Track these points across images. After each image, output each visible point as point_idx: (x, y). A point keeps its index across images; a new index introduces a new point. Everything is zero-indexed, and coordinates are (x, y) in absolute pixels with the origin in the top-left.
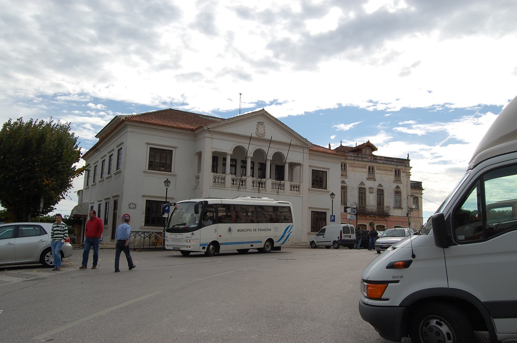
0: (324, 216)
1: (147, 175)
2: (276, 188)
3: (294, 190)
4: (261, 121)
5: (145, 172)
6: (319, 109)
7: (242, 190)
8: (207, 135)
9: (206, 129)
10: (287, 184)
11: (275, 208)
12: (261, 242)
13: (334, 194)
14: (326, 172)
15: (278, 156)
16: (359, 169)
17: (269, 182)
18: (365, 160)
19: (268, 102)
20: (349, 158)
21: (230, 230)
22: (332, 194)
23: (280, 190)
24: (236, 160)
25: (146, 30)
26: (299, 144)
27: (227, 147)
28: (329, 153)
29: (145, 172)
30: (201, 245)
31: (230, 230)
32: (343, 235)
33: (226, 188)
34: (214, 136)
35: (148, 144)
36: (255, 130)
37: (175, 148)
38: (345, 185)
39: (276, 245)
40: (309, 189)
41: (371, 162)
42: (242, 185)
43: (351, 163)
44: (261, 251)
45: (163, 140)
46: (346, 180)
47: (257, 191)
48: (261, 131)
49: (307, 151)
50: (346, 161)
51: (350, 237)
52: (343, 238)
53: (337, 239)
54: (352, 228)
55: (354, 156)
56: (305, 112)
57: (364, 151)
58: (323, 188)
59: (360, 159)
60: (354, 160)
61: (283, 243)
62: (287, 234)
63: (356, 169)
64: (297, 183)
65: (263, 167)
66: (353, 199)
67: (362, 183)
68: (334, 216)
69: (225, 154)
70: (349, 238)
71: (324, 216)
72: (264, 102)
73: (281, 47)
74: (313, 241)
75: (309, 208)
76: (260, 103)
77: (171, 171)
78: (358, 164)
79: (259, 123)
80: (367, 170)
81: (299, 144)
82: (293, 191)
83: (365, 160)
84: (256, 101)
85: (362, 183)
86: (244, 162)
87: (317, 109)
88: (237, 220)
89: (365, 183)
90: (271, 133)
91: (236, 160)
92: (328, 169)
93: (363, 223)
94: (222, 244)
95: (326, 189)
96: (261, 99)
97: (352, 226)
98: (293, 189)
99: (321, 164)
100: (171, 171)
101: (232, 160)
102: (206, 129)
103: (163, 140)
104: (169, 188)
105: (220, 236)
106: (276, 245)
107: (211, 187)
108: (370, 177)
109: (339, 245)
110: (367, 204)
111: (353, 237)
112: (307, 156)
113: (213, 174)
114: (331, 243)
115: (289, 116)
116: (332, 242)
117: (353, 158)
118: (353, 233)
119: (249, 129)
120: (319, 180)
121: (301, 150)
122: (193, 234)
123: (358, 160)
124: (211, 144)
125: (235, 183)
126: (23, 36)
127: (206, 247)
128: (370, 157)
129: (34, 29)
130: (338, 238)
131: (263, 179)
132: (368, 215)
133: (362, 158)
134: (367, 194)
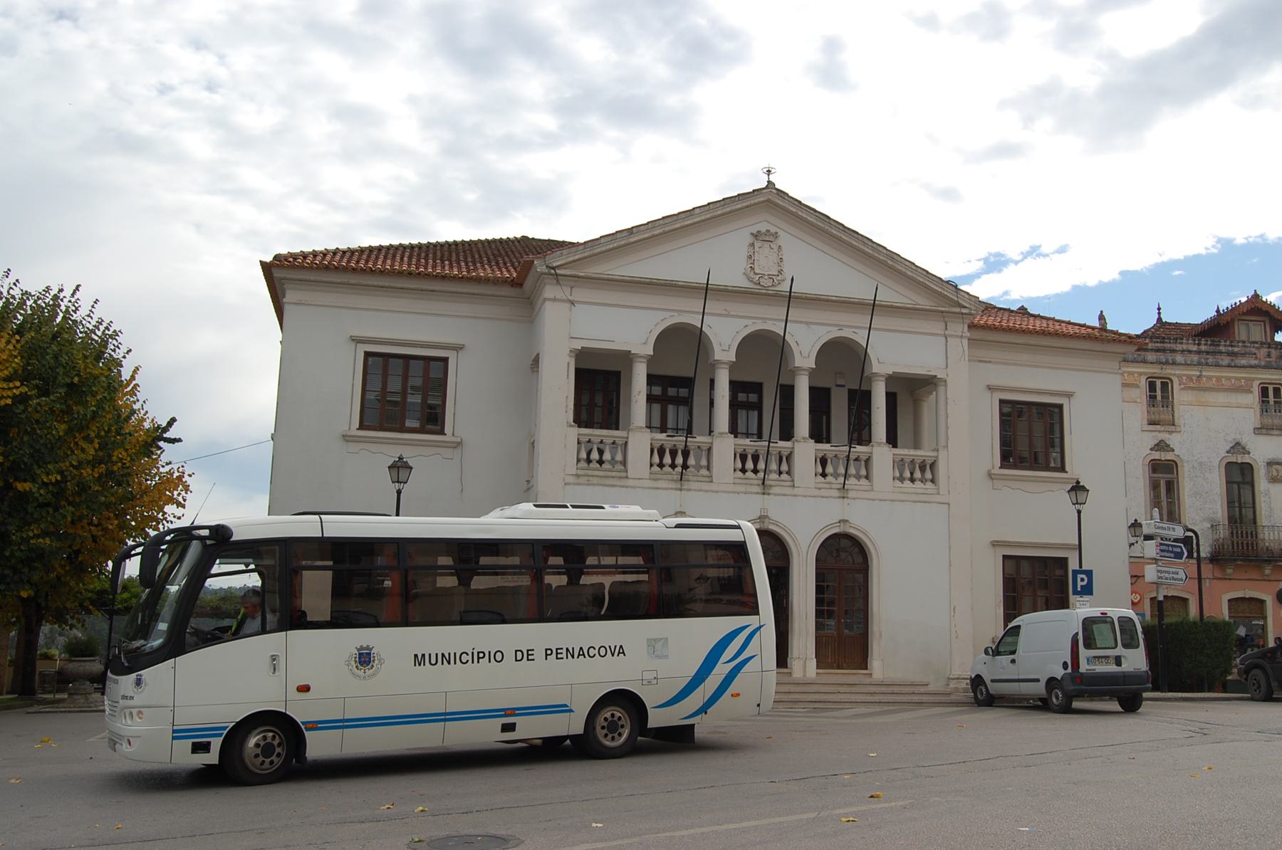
0: (1059, 572)
1: (353, 447)
2: (836, 475)
3: (923, 480)
4: (763, 227)
5: (347, 438)
6: (1165, 259)
7: (693, 485)
8: (550, 291)
9: (544, 269)
10: (882, 455)
11: (645, 551)
12: (563, 709)
13: (1084, 489)
14: (1060, 407)
15: (843, 355)
16: (1221, 398)
17: (639, 439)
18: (1244, 362)
19: (1013, 254)
20: (1179, 358)
21: (365, 658)
22: (1077, 488)
23: (852, 481)
24: (757, 388)
25: (672, 101)
26: (924, 302)
27: (631, 330)
28: (1065, 336)
29: (347, 438)
30: (178, 734)
31: (365, 658)
32: (1084, 653)
33: (630, 482)
34: (579, 294)
35: (357, 341)
36: (743, 264)
37: (458, 348)
38: (1169, 456)
39: (656, 719)
40: (990, 476)
41: (1268, 367)
42: (698, 467)
43: (1190, 378)
44: (576, 749)
45: (410, 325)
46: (1173, 440)
47: (758, 489)
48: (766, 261)
49: (959, 328)
50: (1169, 371)
51: (1118, 661)
52: (1084, 667)
53: (1059, 673)
54: (1126, 623)
55: (1199, 352)
56: (1122, 273)
57: (1241, 331)
58: (1048, 469)
59: (1226, 360)
60: (1199, 364)
61: (704, 709)
62: (721, 670)
63: (1211, 397)
64: (924, 453)
65: (746, 395)
66: (1204, 505)
67: (1238, 447)
68: (1089, 573)
69: (627, 358)
70: (1112, 668)
71: (1059, 572)
72: (1002, 255)
73: (1043, 99)
74: (978, 676)
75: (995, 544)
76: (992, 259)
77: (442, 432)
78: (1219, 379)
79: (756, 236)
80: (1253, 398)
81: (924, 302)
82: (918, 484)
83: (1244, 362)
84: (983, 255)
85: (1238, 447)
86: (787, 394)
87: (1159, 260)
88: (413, 608)
89: (1249, 447)
90: (811, 271)
91: (757, 388)
92: (1069, 395)
93: (1249, 594)
94: (314, 726)
95: (1062, 469)
96: (993, 250)
97: (1130, 613)
98: (918, 474)
99: (1034, 378)
100: (442, 432)
101: (735, 386)
102: (544, 269)
103: (410, 325)
104: (406, 489)
105: (305, 689)
106: (656, 719)
107: (571, 479)
108: (1268, 421)
109: (1069, 698)
110: (1263, 520)
111: (1136, 660)
112: (959, 347)
113: (575, 432)
114: (1040, 689)
115: (1075, 287)
116: (1042, 684)
117: (1195, 358)
118: (1130, 644)
119: (723, 260)
120: (1031, 437)
121: (937, 327)
122: (139, 682)
123: (1217, 365)
124: (577, 323)
125: (829, 469)
126: (380, 150)
127: (216, 744)
128: (1264, 351)
129: (404, 130)
130: (1065, 665)
131: (859, 448)
132: (1268, 561)
133: (1232, 354)
134: (1262, 483)
